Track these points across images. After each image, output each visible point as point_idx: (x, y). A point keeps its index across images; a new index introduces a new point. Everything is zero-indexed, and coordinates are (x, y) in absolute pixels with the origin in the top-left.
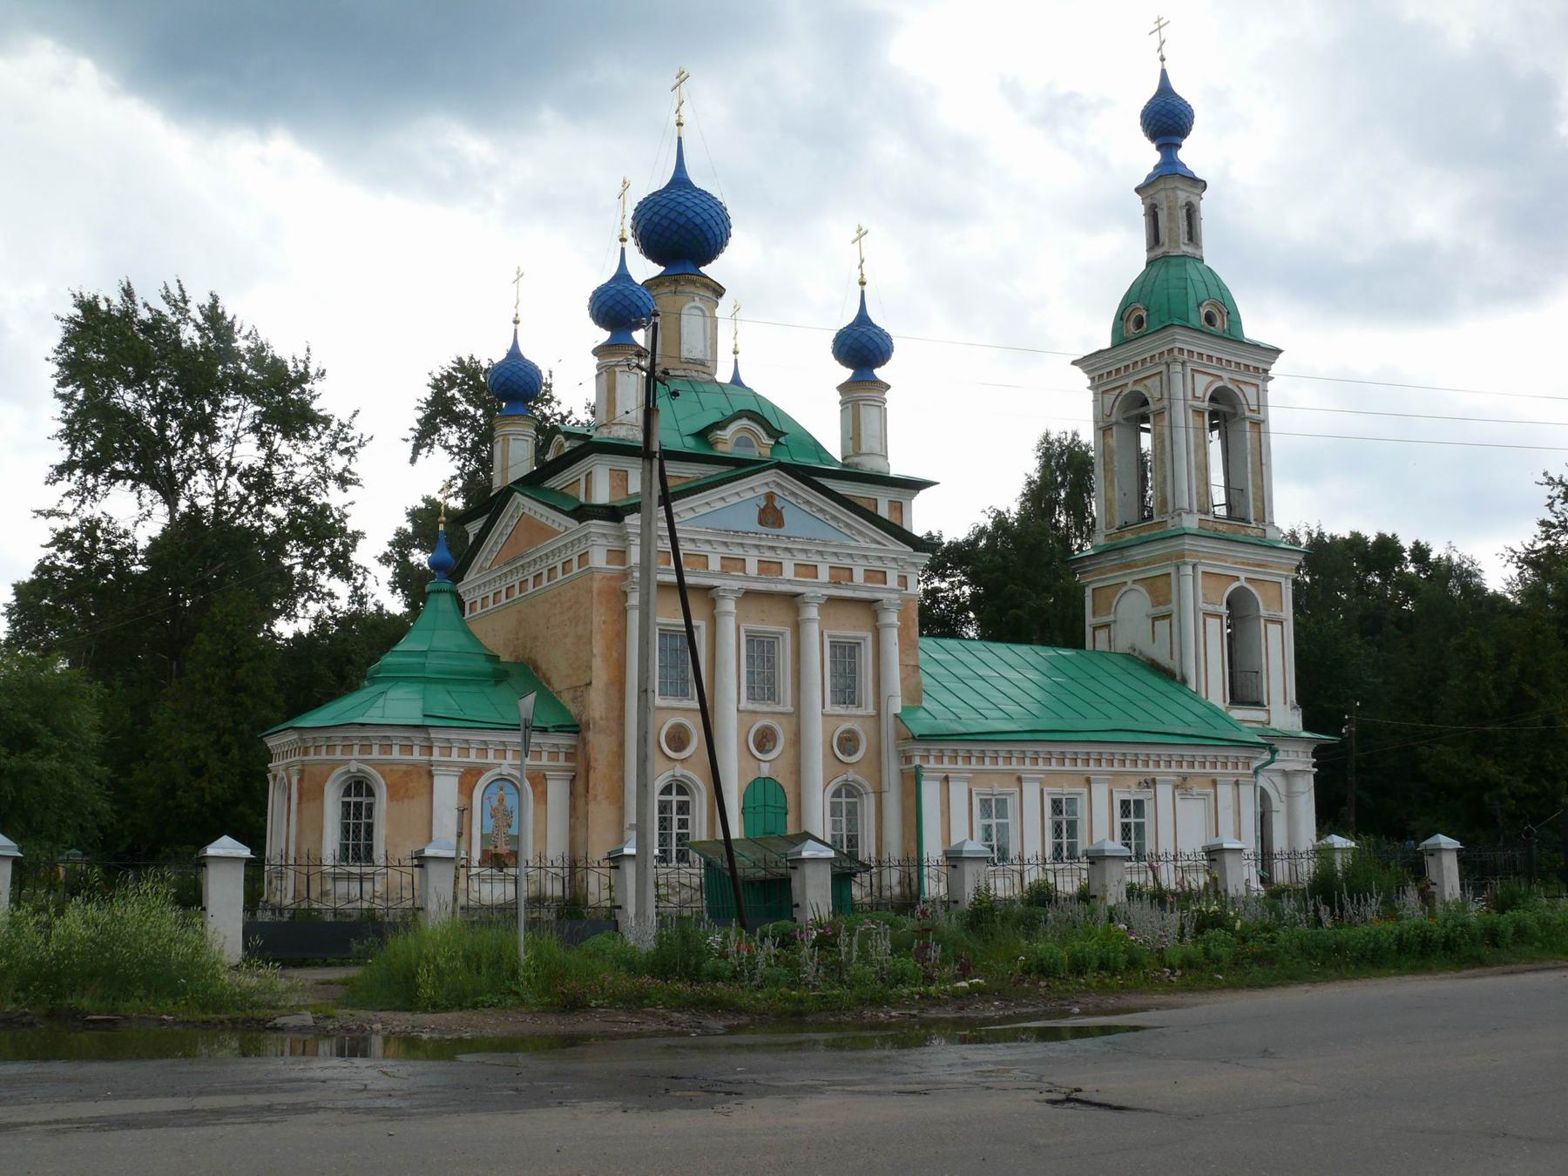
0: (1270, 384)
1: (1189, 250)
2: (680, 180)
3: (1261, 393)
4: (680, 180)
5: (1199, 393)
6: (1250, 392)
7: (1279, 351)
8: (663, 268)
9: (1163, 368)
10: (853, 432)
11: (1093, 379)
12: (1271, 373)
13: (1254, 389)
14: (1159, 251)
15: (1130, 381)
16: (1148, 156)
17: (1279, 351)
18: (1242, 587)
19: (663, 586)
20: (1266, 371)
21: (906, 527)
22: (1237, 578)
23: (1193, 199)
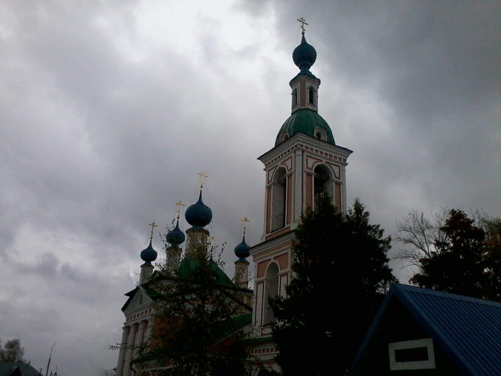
0: (347, 167)
1: (310, 107)
2: (200, 202)
3: (342, 172)
4: (200, 202)
5: (310, 166)
6: (336, 169)
7: (352, 152)
8: (191, 226)
9: (293, 154)
10: (238, 275)
11: (266, 165)
12: (347, 162)
13: (338, 168)
14: (299, 107)
15: (279, 163)
16: (297, 70)
17: (352, 152)
18: (323, 165)
19: (180, 213)
20: (345, 160)
21: (251, 307)
22: (321, 161)
23: (314, 86)
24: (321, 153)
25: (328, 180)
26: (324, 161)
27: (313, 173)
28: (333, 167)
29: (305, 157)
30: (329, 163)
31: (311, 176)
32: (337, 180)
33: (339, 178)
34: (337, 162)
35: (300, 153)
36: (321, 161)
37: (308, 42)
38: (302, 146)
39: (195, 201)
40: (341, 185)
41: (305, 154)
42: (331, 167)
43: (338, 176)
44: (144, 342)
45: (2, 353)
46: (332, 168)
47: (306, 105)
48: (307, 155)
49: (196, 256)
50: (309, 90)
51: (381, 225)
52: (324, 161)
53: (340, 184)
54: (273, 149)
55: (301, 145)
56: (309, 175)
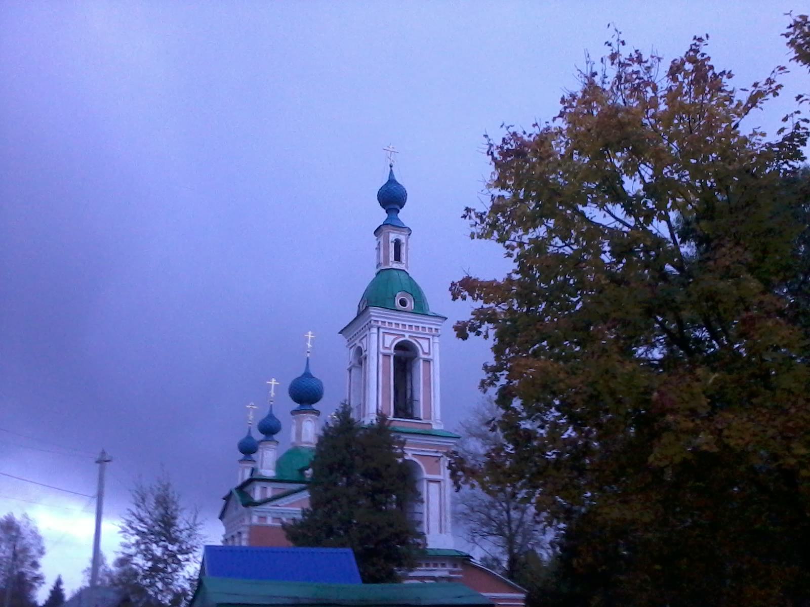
1: (395, 266)
2: (307, 375)
4: (307, 375)
5: (387, 345)
6: (425, 344)
13: (427, 341)
22: (404, 336)
24: (404, 325)
25: (416, 357)
26: (407, 335)
27: (392, 354)
28: (420, 341)
29: (381, 334)
30: (415, 337)
31: (390, 356)
32: (426, 357)
33: (429, 354)
34: (427, 334)
35: (375, 330)
36: (404, 336)
37: (398, 179)
38: (378, 321)
39: (300, 373)
40: (432, 363)
41: (381, 330)
42: (416, 341)
43: (426, 351)
44: (599, 511)
45: (467, 522)
46: (419, 343)
47: (391, 264)
48: (383, 332)
49: (530, 352)
50: (393, 244)
51: (62, 574)
52: (407, 335)
53: (430, 362)
54: (355, 319)
55: (375, 321)
56: (385, 355)
